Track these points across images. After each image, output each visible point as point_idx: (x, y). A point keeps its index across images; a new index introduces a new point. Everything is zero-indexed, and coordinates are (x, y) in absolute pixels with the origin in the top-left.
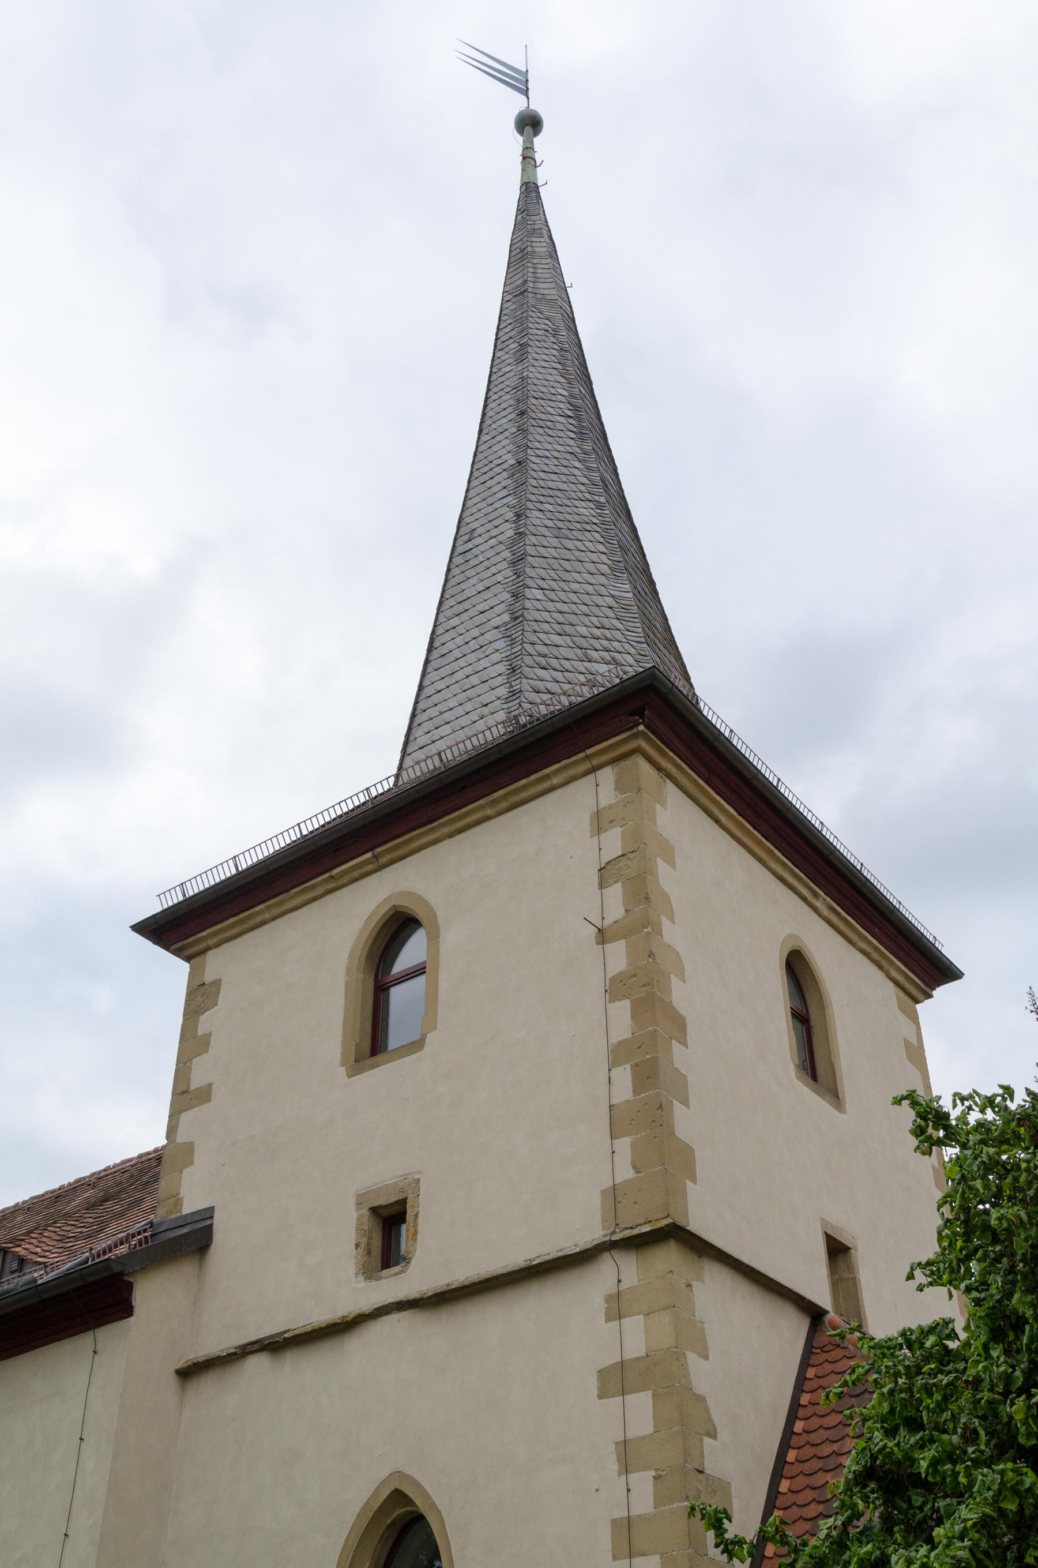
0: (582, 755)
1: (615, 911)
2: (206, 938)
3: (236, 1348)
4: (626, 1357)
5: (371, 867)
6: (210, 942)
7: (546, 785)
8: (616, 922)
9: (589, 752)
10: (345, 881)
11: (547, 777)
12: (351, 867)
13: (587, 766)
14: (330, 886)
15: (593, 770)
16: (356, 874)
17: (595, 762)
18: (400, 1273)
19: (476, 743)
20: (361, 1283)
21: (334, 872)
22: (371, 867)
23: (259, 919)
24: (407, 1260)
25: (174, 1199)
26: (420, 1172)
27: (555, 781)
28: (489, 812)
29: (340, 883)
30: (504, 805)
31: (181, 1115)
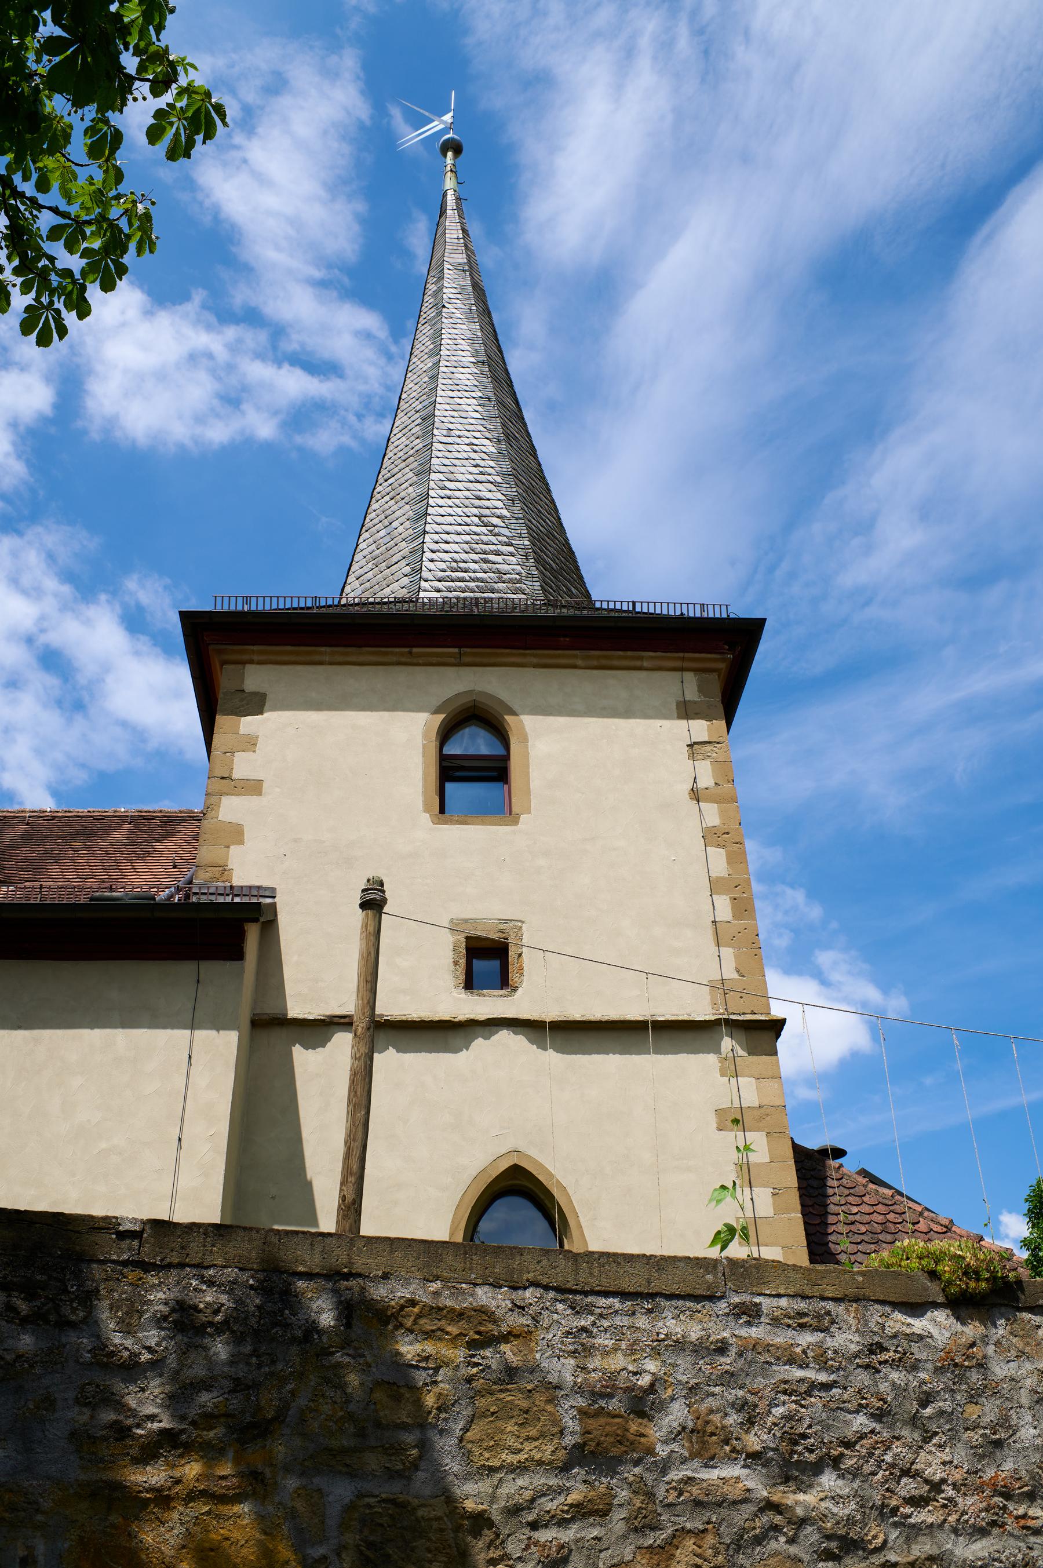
0: (681, 655)
1: (706, 781)
2: (253, 652)
3: (326, 1016)
4: (188, 1032)
5: (452, 660)
6: (256, 658)
7: (638, 663)
8: (707, 789)
9: (687, 655)
10: (421, 662)
11: (641, 658)
12: (449, 653)
13: (678, 664)
14: (403, 659)
15: (682, 669)
16: (434, 660)
17: (686, 664)
18: (508, 996)
19: (685, 611)
20: (462, 995)
21: (415, 650)
22: (452, 660)
23: (317, 658)
24: (515, 989)
25: (221, 868)
26: (523, 922)
27: (645, 664)
28: (579, 662)
29: (415, 661)
30: (595, 663)
31: (223, 798)
